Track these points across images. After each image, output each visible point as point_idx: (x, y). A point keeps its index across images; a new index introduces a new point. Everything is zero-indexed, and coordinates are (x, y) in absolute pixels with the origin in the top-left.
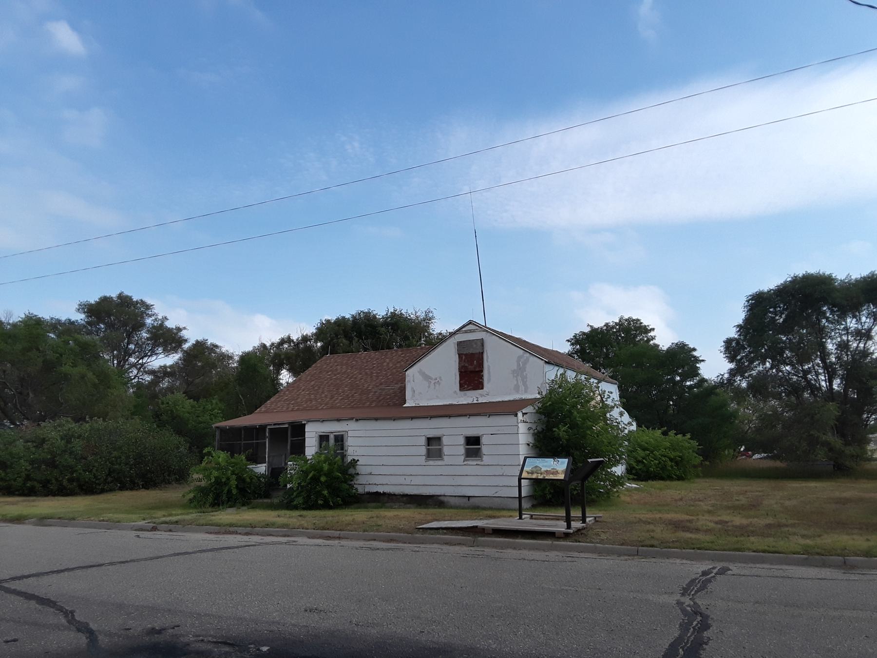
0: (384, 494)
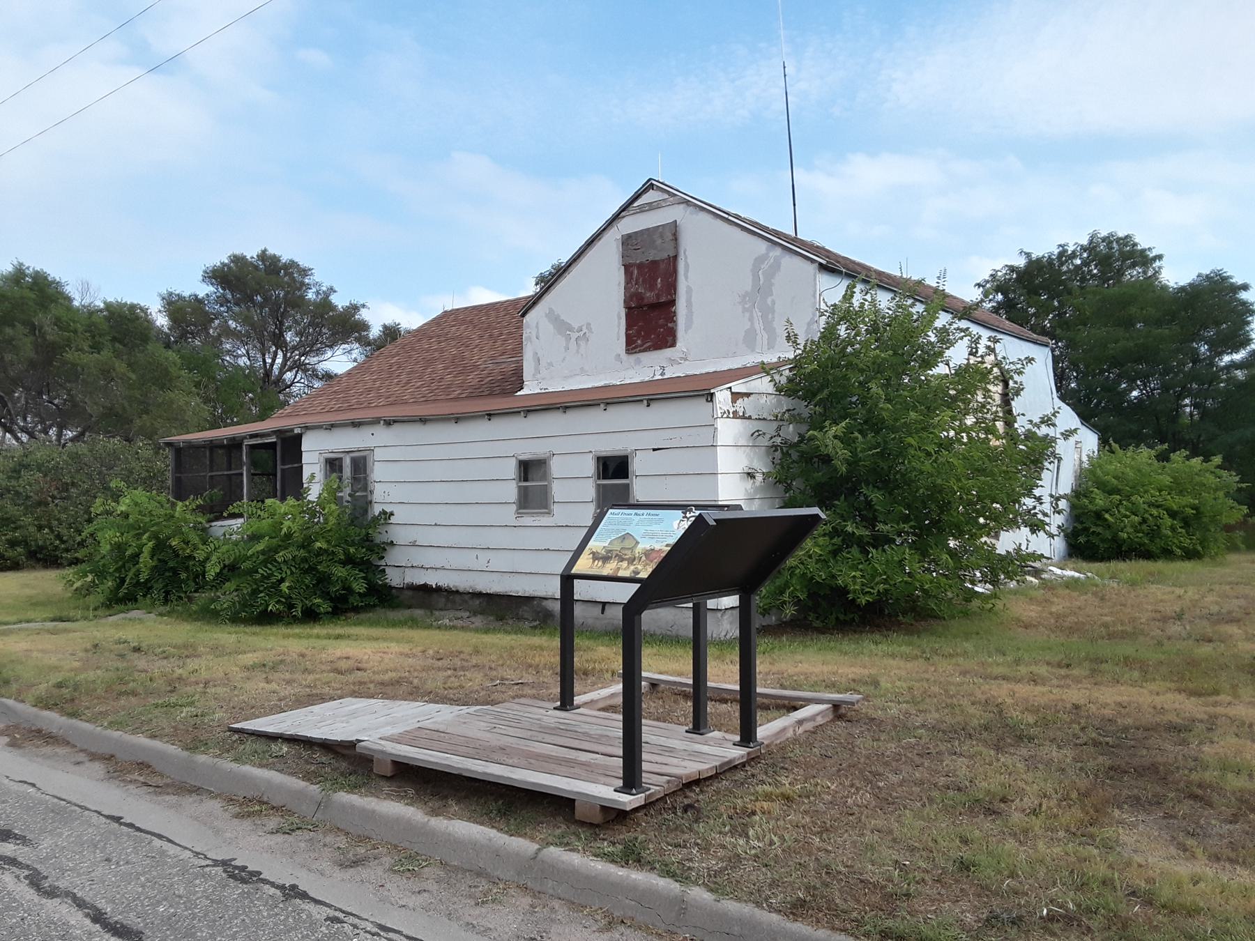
0: (439, 589)
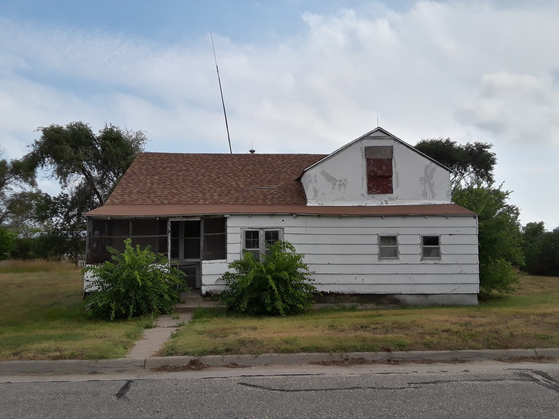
0: (331, 294)
